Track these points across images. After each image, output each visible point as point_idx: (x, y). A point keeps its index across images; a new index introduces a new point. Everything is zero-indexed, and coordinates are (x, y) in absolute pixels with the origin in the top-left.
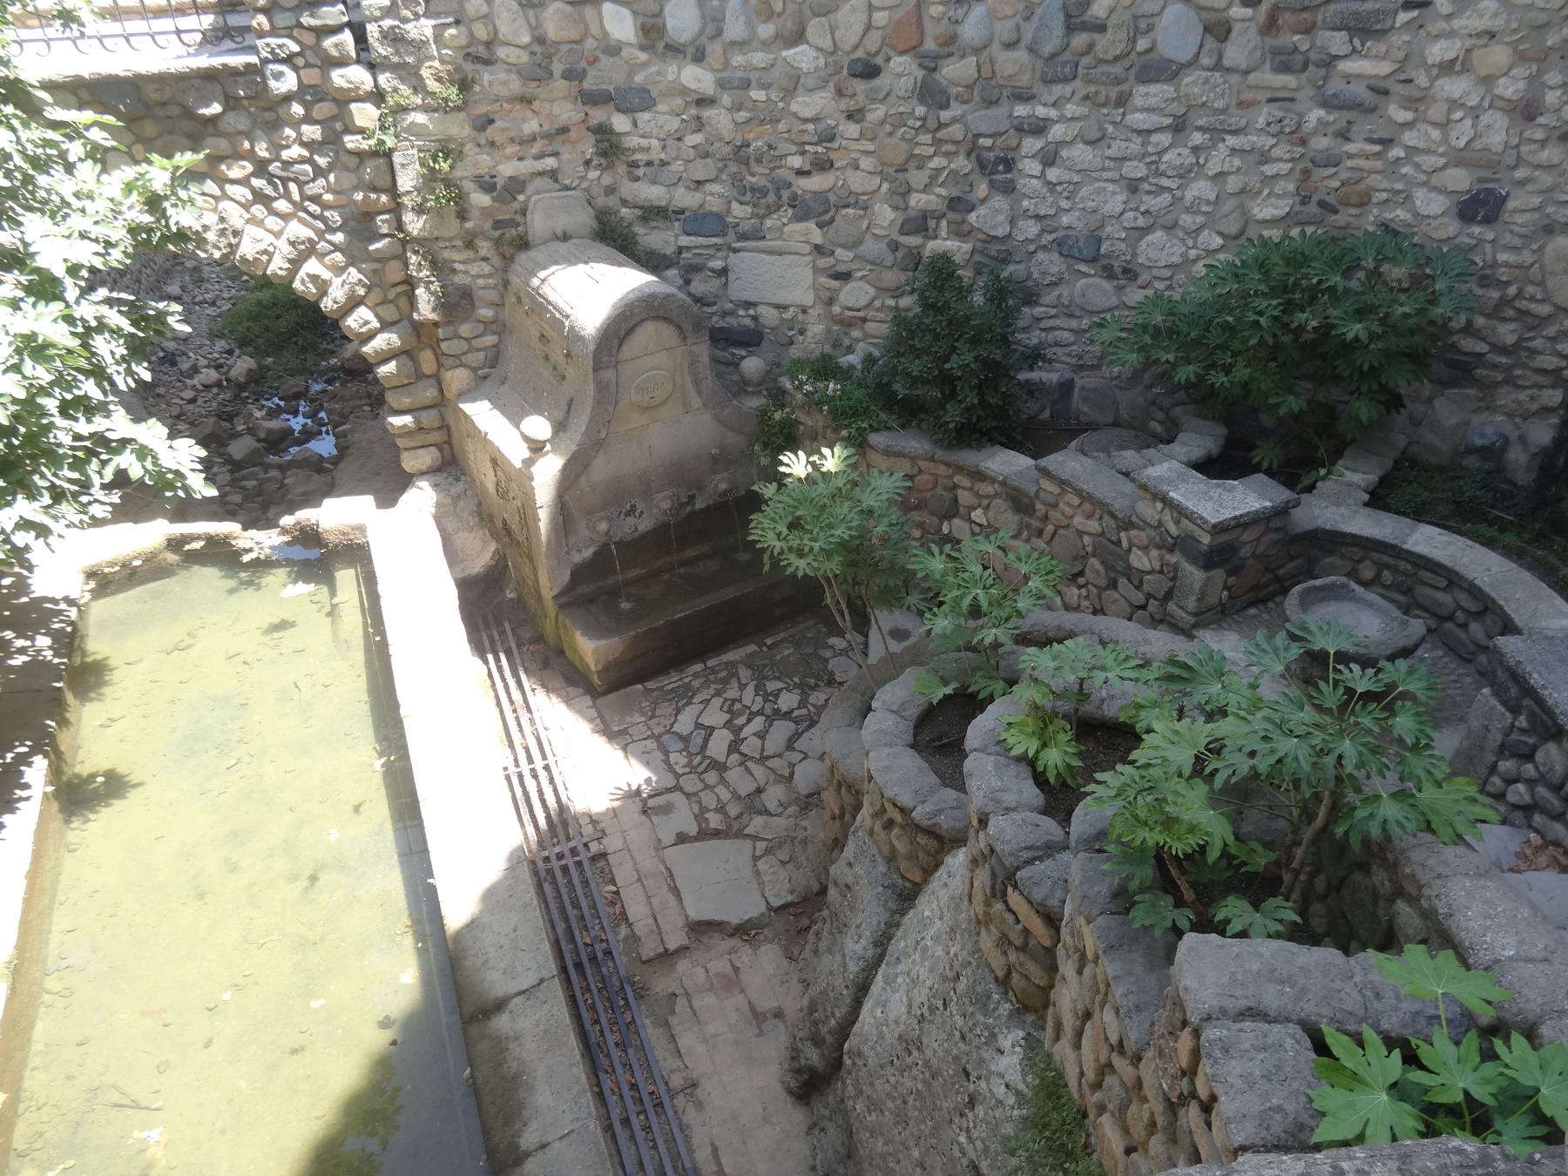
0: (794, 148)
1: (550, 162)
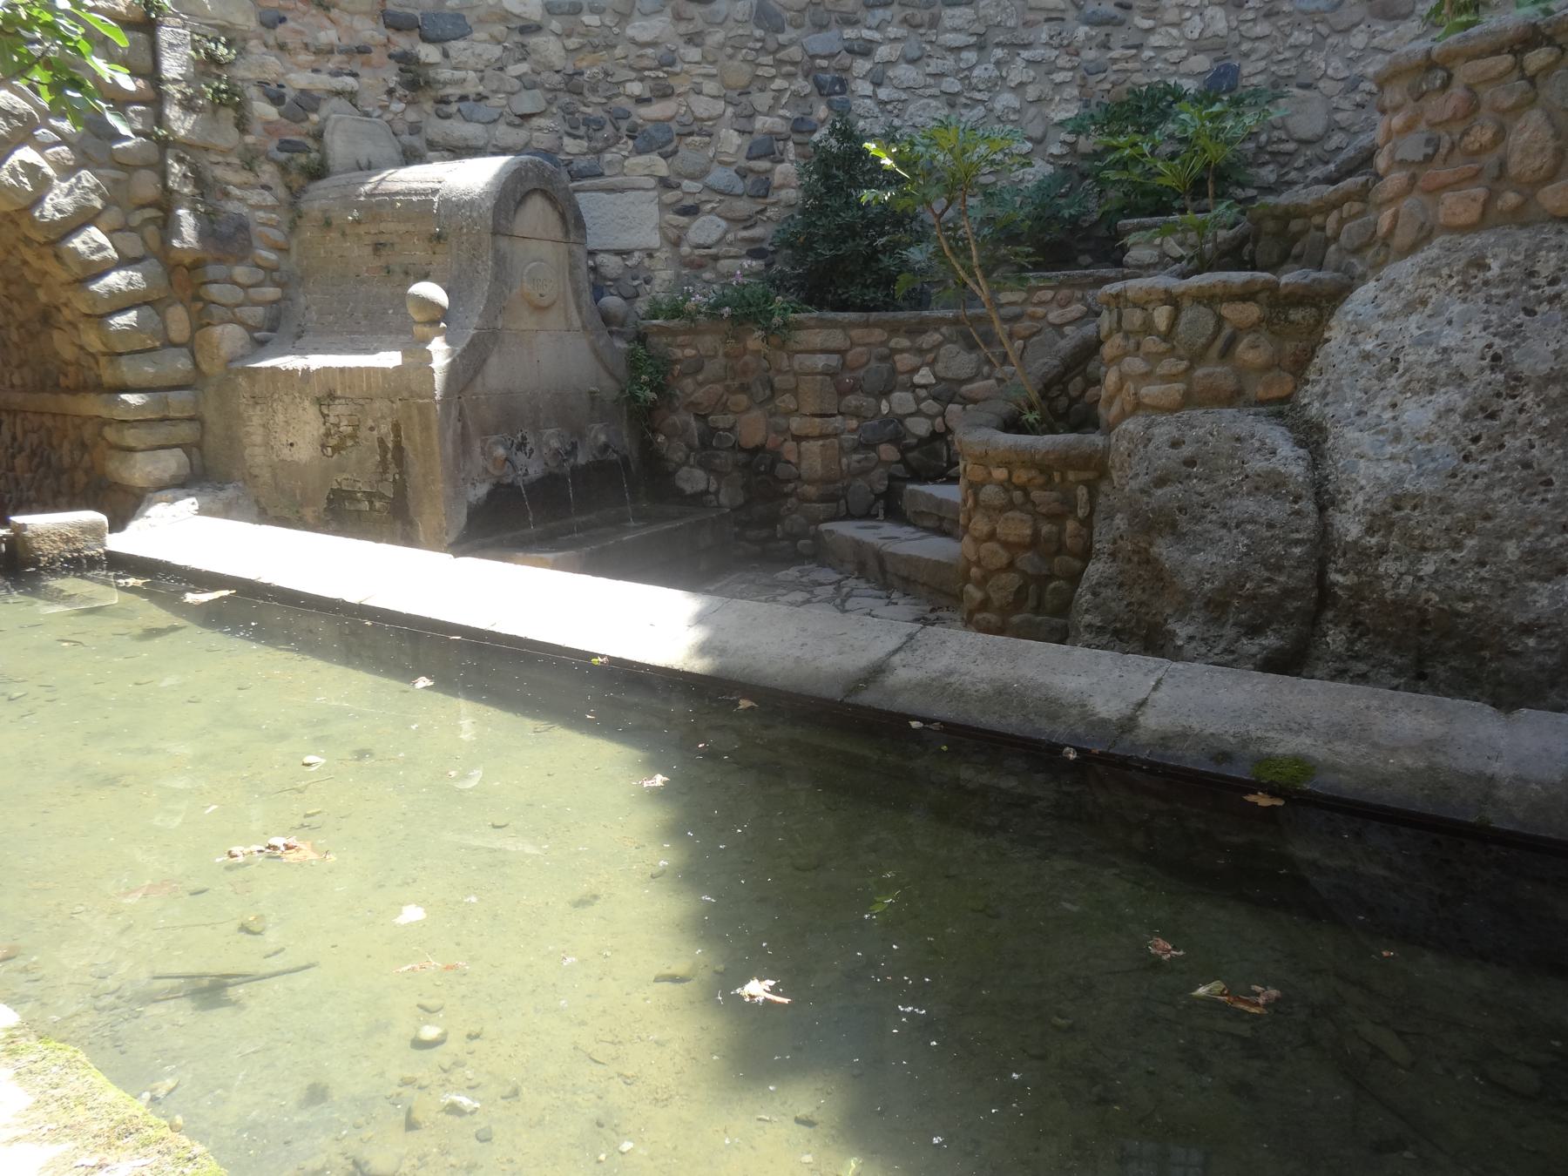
0: (633, 75)
1: (349, 82)
